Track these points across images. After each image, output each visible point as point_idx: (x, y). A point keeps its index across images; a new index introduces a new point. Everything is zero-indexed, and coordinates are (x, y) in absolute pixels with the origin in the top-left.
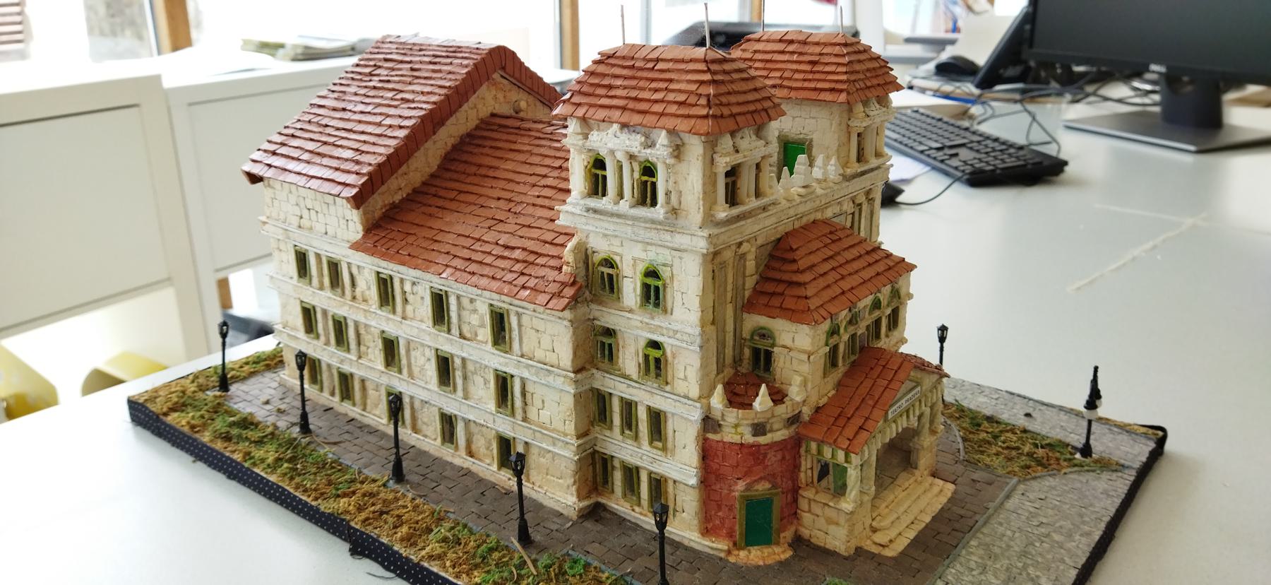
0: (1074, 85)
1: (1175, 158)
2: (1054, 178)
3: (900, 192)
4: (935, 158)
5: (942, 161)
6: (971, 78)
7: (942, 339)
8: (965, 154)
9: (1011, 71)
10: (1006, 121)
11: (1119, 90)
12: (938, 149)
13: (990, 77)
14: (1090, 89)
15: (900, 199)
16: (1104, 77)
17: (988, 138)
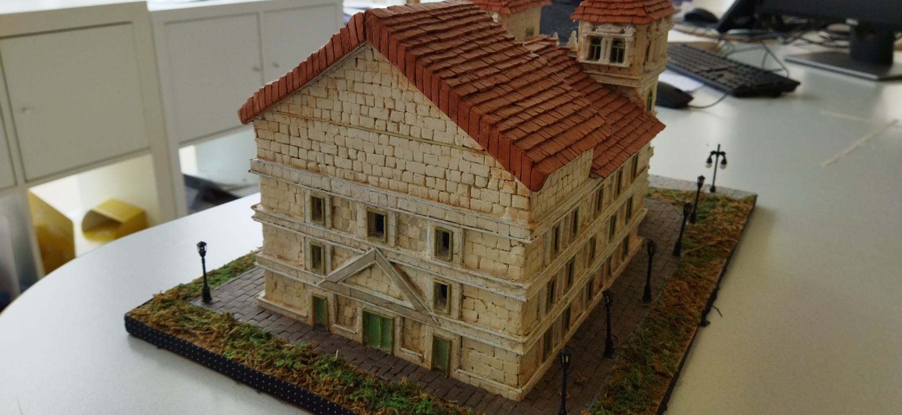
0: (786, 31)
1: (858, 82)
2: (790, 94)
3: (691, 98)
4: (707, 78)
5: (713, 80)
6: (713, 25)
7: (203, 253)
8: (727, 75)
9: (742, 20)
10: (748, 54)
11: (814, 36)
12: (709, 71)
13: (726, 24)
14: (797, 34)
15: (692, 103)
16: (806, 28)
17: (741, 65)
